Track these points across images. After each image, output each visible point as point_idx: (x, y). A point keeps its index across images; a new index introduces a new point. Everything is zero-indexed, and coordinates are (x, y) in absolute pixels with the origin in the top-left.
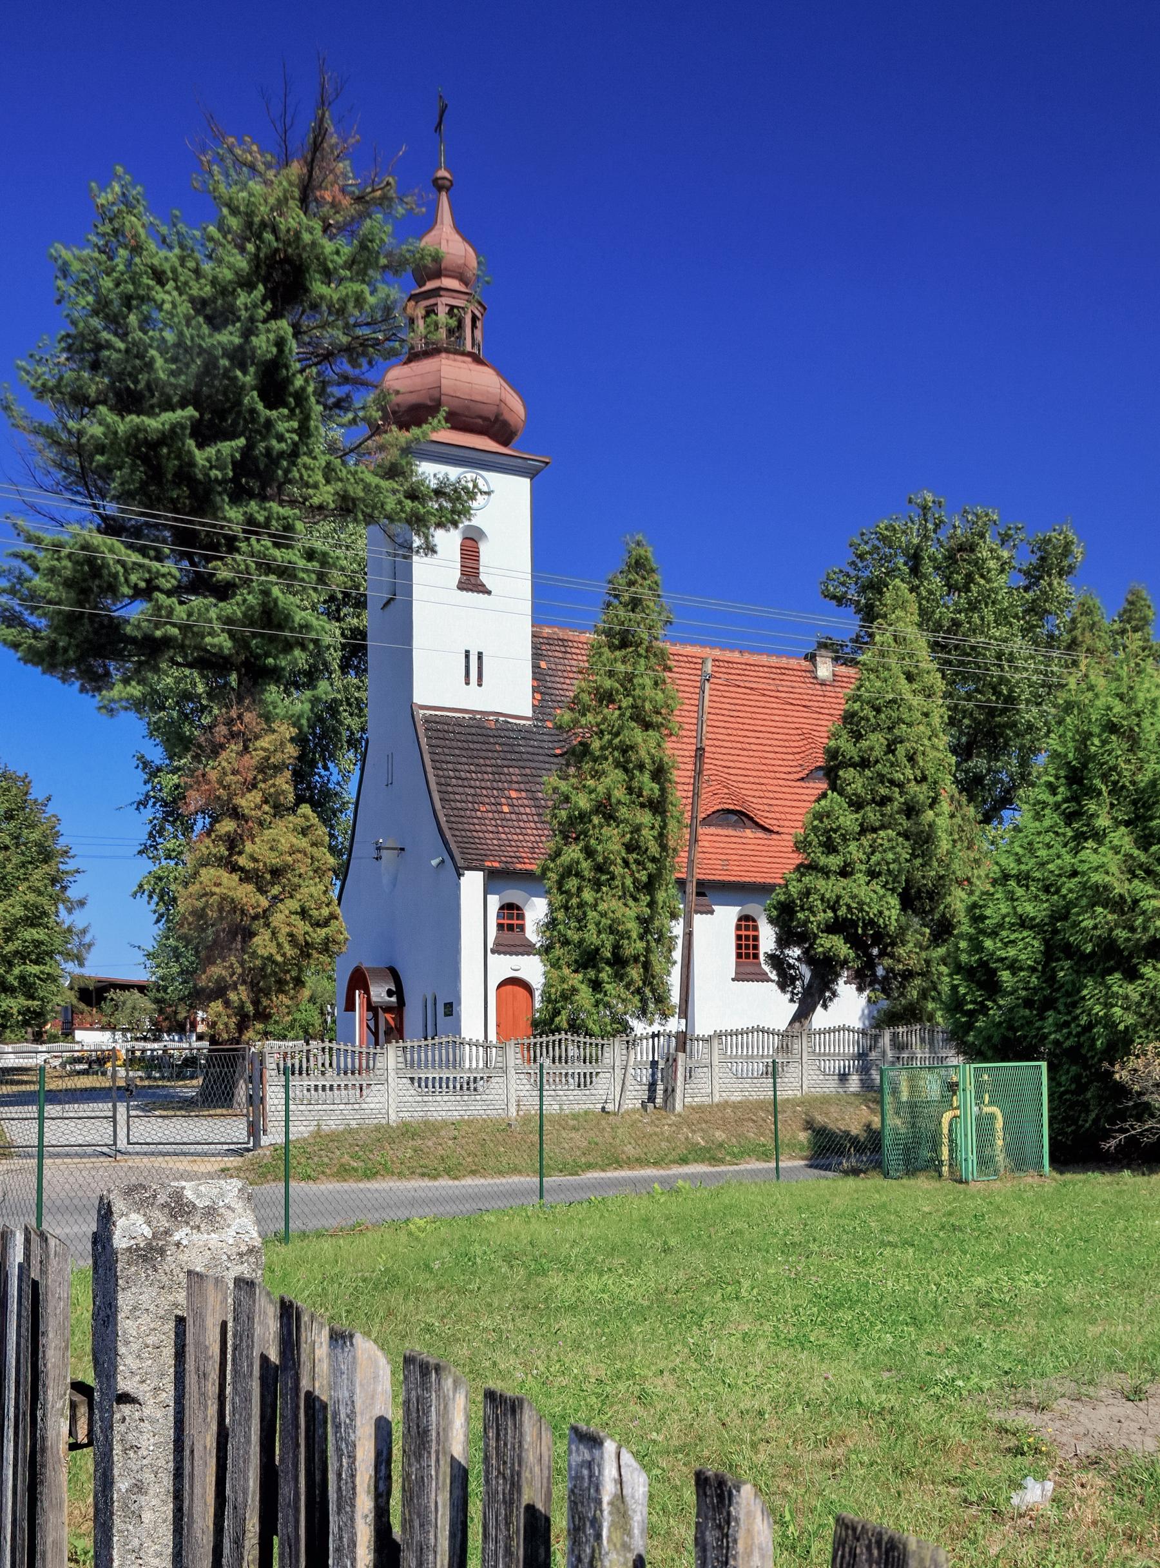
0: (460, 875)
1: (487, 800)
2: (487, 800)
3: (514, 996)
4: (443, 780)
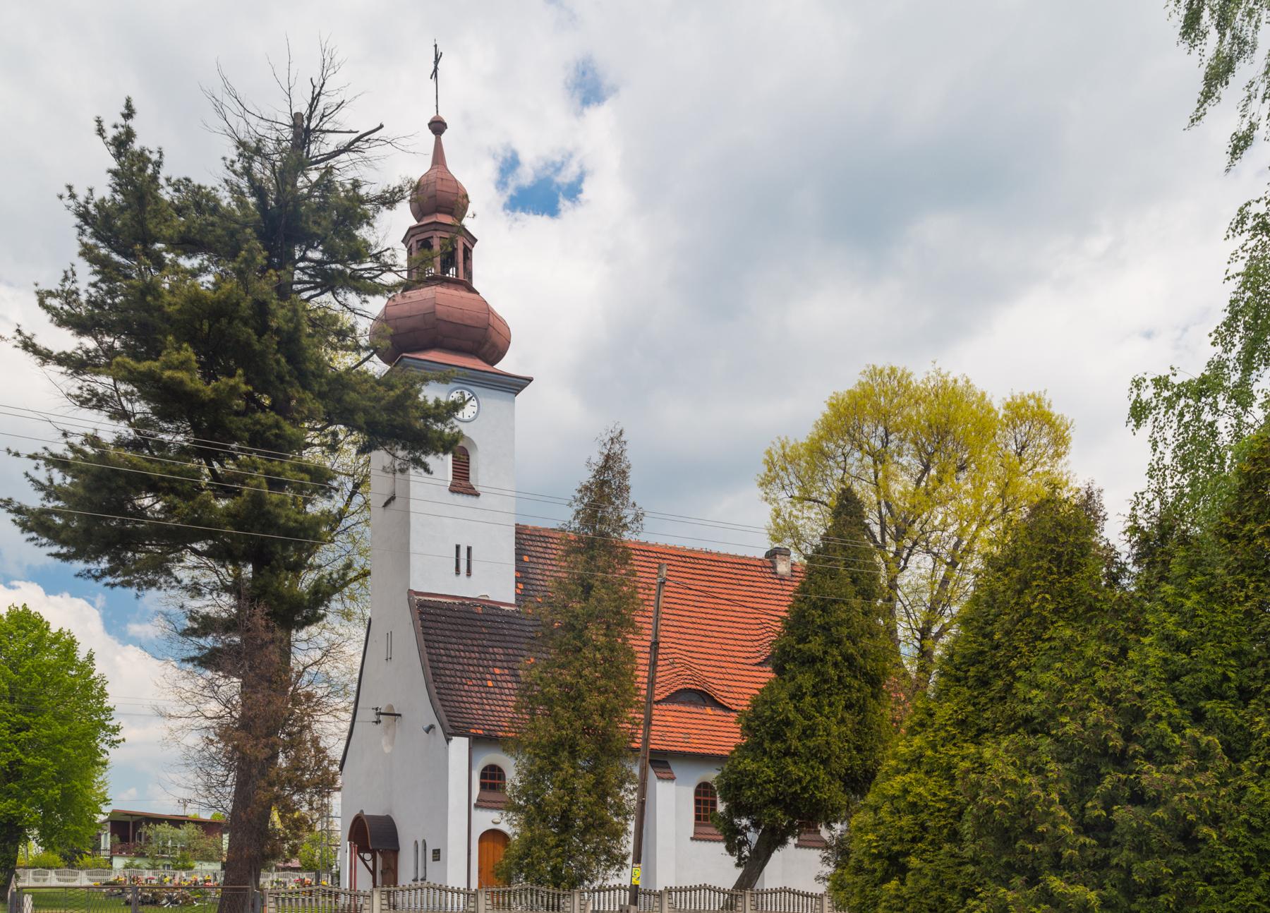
0: (448, 740)
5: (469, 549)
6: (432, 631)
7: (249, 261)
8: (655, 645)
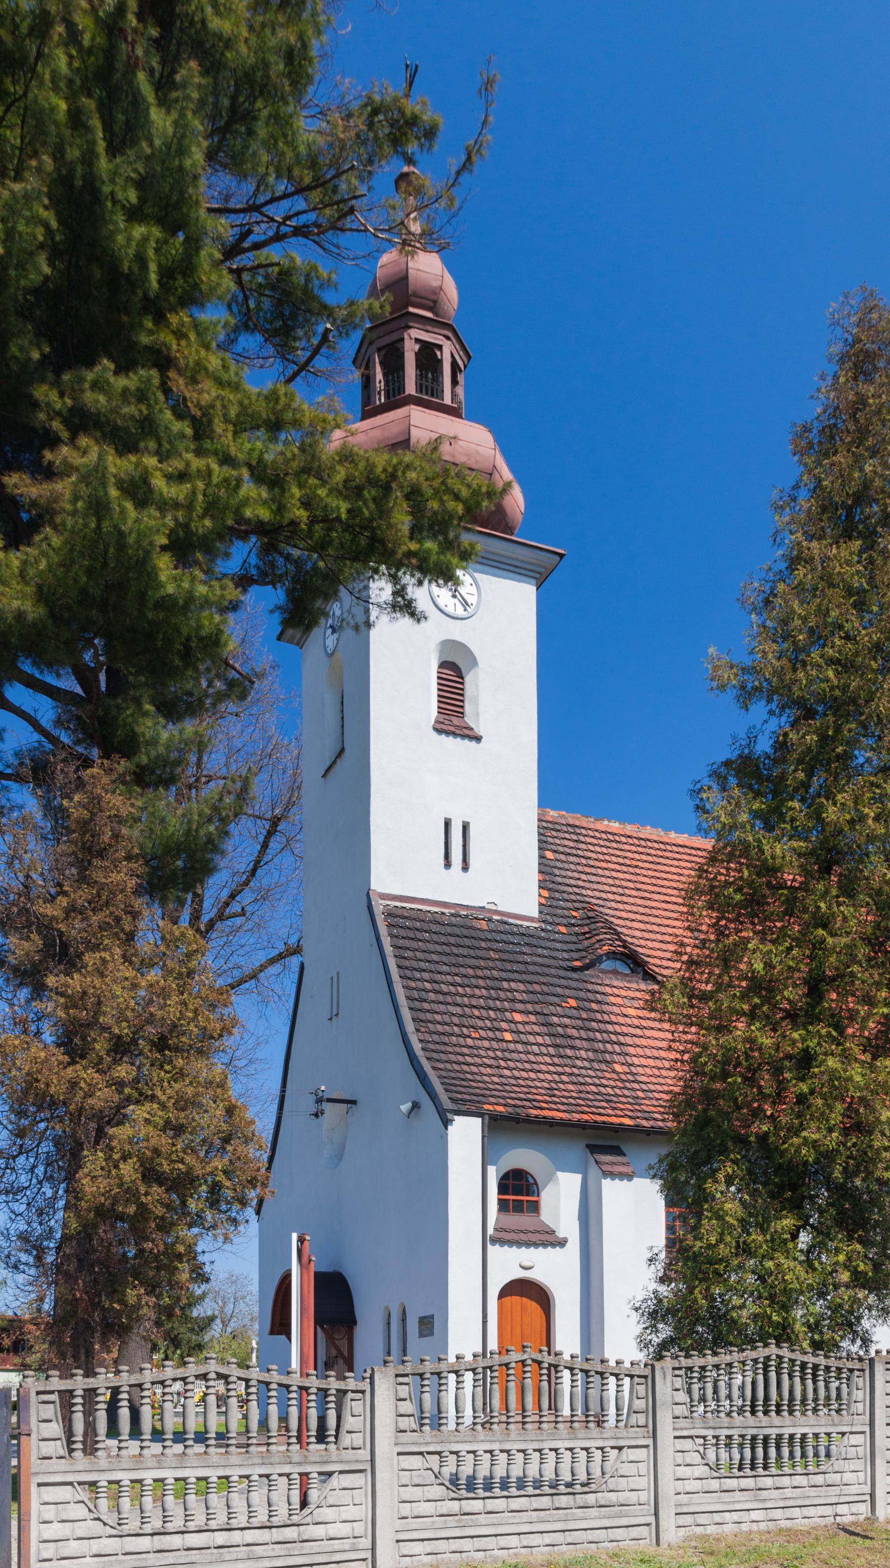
0: (446, 1123)
1: (480, 1023)
2: (480, 1023)
3: (523, 1309)
4: (415, 994)
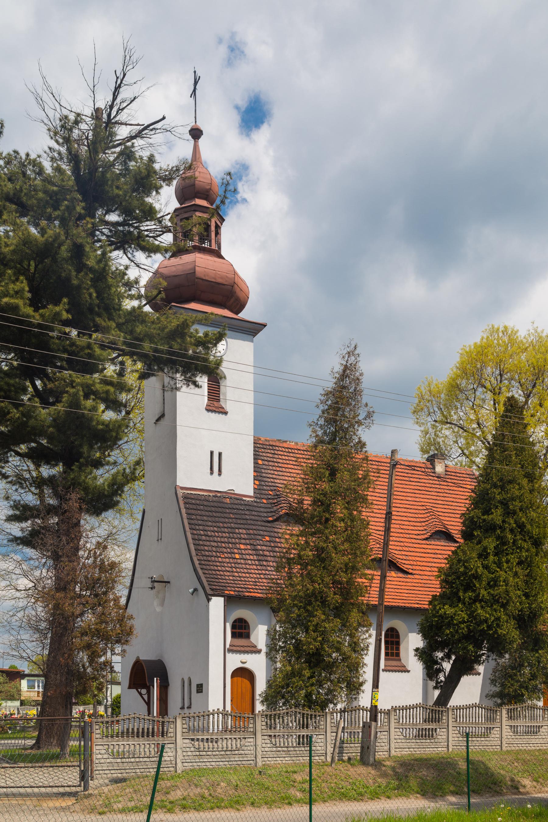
0: (209, 600)
5: (220, 454)
6: (194, 517)
7: (70, 209)
8: (389, 515)
